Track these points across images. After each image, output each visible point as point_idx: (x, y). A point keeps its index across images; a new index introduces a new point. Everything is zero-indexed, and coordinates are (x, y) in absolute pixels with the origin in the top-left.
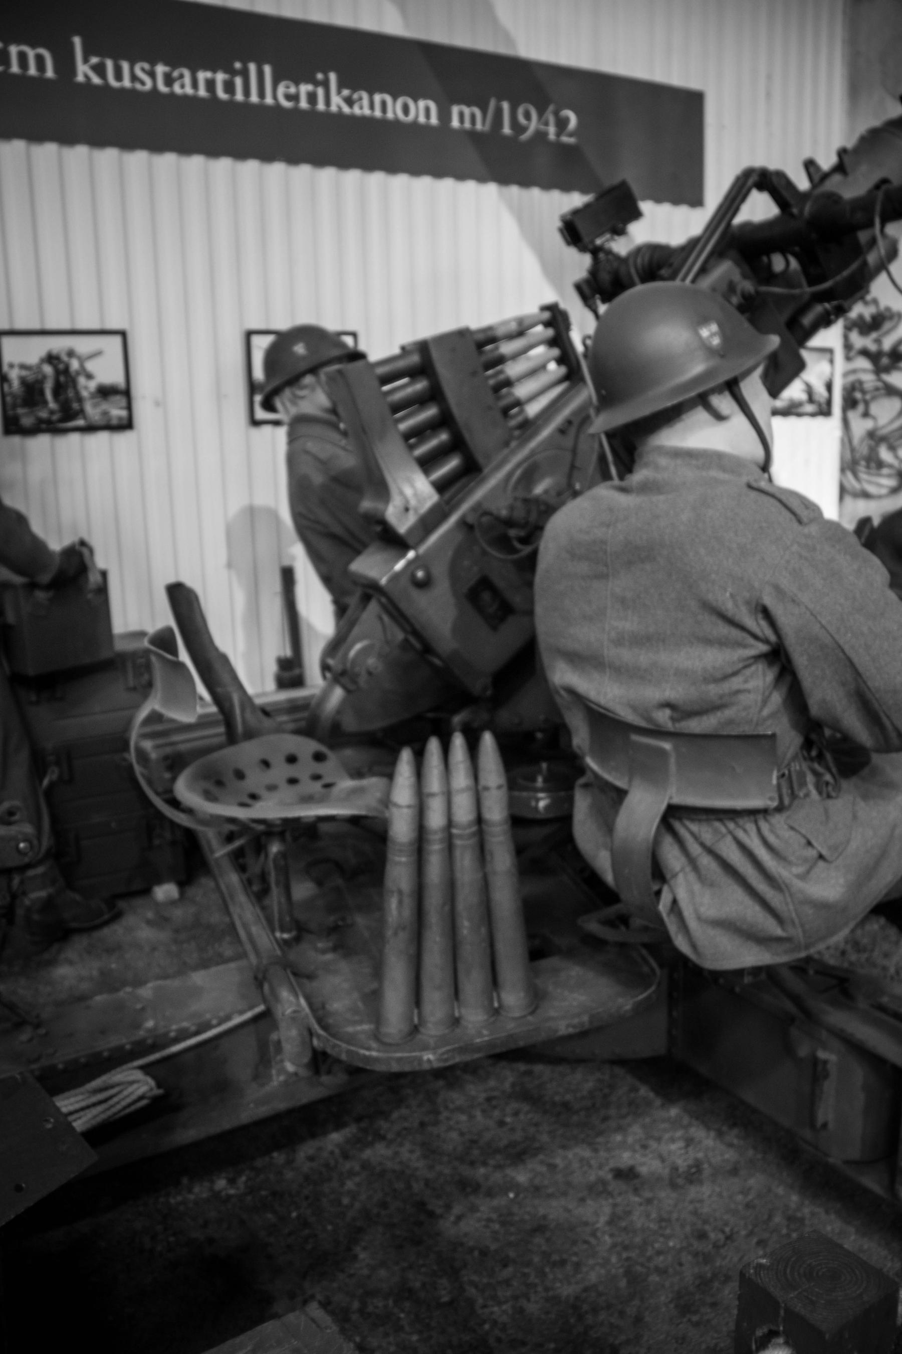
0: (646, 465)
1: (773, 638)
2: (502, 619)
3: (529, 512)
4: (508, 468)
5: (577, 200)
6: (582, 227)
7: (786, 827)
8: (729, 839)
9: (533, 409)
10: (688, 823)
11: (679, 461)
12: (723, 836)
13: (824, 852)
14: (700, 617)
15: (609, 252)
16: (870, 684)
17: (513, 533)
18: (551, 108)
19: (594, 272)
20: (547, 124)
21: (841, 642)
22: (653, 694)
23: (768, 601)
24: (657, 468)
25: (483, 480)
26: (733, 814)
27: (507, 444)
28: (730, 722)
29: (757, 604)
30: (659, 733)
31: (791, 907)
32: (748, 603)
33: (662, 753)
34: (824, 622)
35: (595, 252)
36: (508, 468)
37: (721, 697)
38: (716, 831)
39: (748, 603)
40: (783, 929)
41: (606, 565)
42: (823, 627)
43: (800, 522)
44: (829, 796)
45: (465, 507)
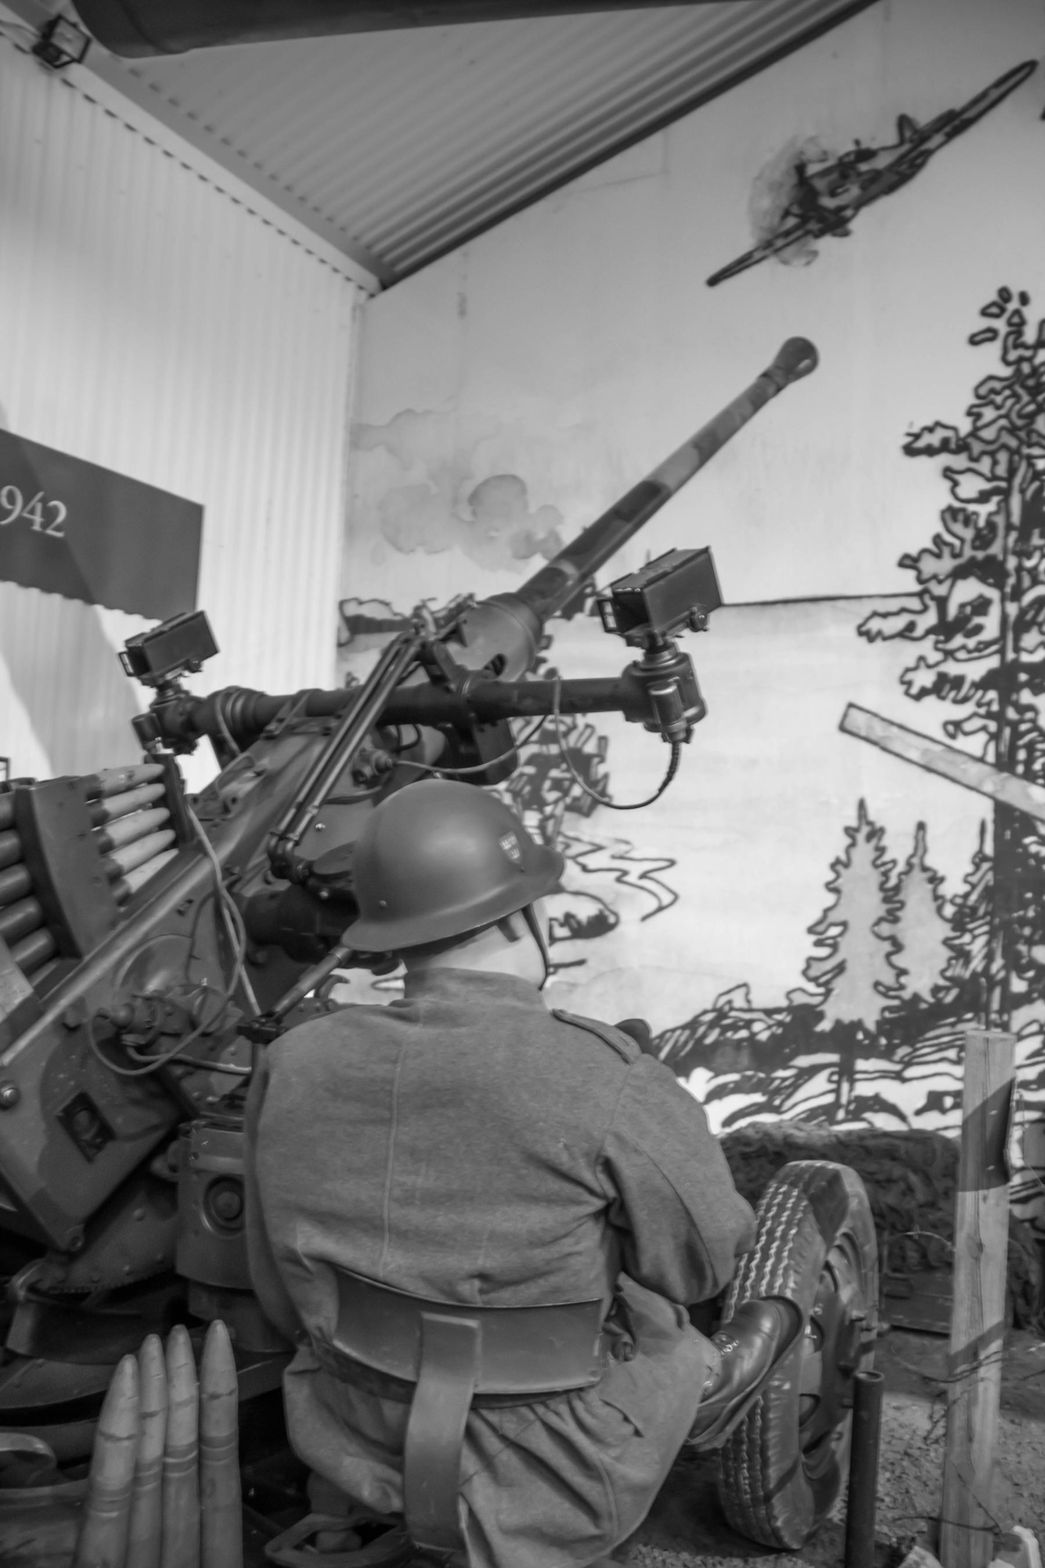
0: (430, 990)
1: (611, 1193)
2: (99, 1148)
3: (153, 1014)
4: (116, 955)
5: (145, 625)
6: (151, 656)
7: (601, 1403)
8: (538, 1426)
9: (135, 881)
10: (485, 1413)
11: (471, 987)
12: (531, 1423)
13: (640, 1426)
14: (524, 1172)
15: (178, 689)
16: (704, 1234)
17: (129, 1039)
18: (40, 495)
19: (158, 708)
20: (32, 512)
21: (680, 1191)
22: (456, 1263)
23: (612, 1151)
24: (445, 993)
25: (85, 969)
26: (552, 1394)
27: (113, 924)
28: (556, 1290)
29: (598, 1156)
30: (464, 1309)
31: (611, 1498)
32: (587, 1155)
33: (468, 1331)
34: (665, 1172)
35: (162, 688)
36: (116, 955)
37: (548, 1262)
38: (522, 1419)
39: (587, 1155)
40: (597, 1525)
41: (390, 1109)
42: (664, 1177)
43: (626, 1061)
44: (626, 1359)
45: (64, 1002)
